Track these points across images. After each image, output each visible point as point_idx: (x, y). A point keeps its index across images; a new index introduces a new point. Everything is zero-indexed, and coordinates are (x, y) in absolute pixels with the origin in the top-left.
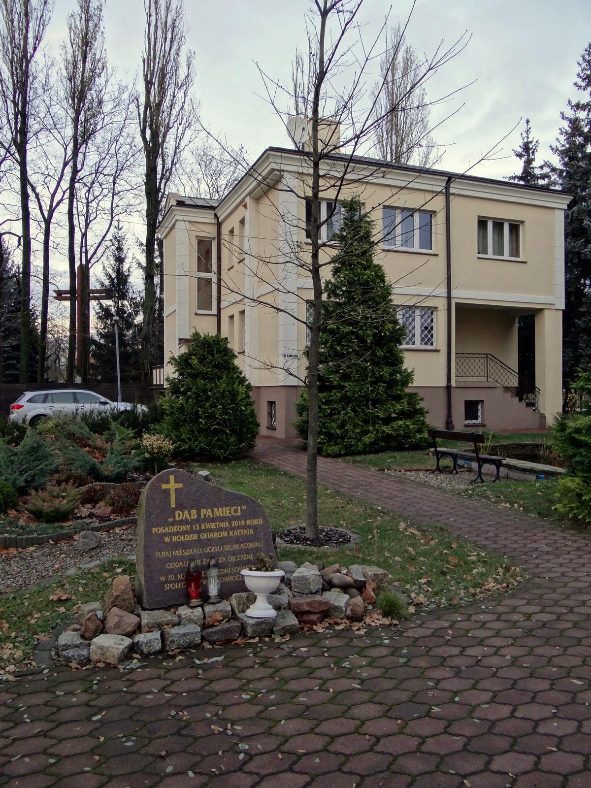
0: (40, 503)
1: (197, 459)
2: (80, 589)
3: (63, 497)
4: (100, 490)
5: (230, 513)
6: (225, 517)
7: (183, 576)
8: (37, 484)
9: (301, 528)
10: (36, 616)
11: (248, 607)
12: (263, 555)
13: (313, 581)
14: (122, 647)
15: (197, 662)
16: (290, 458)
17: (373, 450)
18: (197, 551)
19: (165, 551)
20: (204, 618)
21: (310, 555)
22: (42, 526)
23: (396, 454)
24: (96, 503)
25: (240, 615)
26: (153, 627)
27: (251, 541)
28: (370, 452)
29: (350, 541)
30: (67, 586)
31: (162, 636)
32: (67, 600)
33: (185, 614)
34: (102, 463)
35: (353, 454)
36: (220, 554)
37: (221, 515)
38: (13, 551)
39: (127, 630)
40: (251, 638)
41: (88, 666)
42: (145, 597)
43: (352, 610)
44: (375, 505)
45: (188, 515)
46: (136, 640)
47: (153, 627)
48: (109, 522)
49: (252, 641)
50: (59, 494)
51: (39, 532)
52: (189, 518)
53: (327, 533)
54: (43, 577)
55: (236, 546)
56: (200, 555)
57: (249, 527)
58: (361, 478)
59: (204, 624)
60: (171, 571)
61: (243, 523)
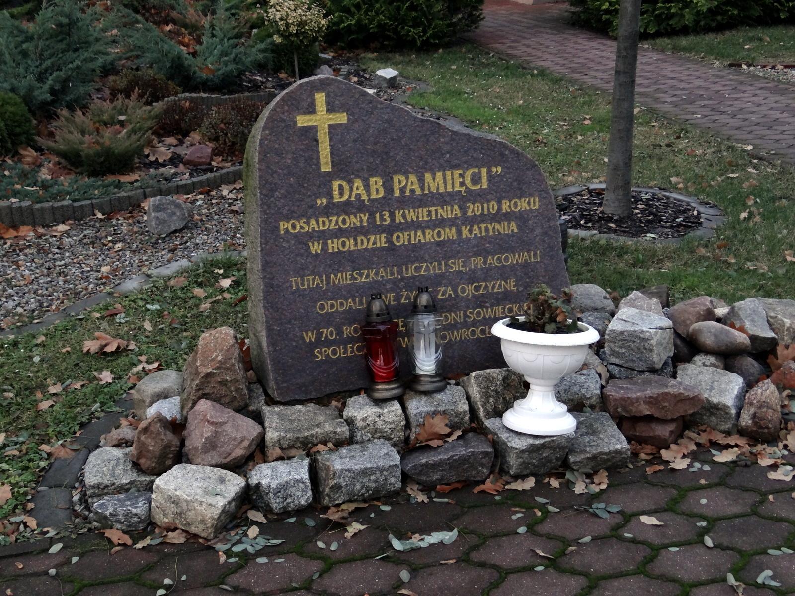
0: (76, 136)
1: (373, 45)
2: (147, 326)
3: (122, 124)
4: (191, 109)
5: (462, 184)
6: (450, 194)
7: (355, 330)
8: (72, 96)
9: (590, 192)
10: (52, 390)
11: (508, 405)
12: (549, 292)
13: (659, 343)
14: (220, 502)
15: (397, 545)
16: (548, 43)
17: (714, 25)
18: (384, 274)
19: (313, 273)
20: (408, 426)
21: (620, 256)
22: (80, 183)
23: (759, 32)
24: (186, 134)
25: (489, 423)
26: (291, 447)
27: (512, 250)
28: (707, 30)
29: (700, 224)
30: (120, 318)
31: (314, 472)
32: (118, 352)
33: (364, 419)
34: (194, 54)
35: (672, 33)
36: (438, 280)
37: (442, 190)
38: (27, 232)
39: (233, 456)
40: (516, 477)
41: (147, 541)
42: (271, 376)
43: (754, 416)
44: (738, 141)
45: (361, 190)
46: (254, 481)
47: (291, 447)
48: (209, 175)
49: (519, 486)
50: (112, 118)
51: (76, 195)
52: (364, 197)
53: (647, 202)
54: (77, 294)
55: (477, 262)
56: (394, 282)
57: (508, 217)
58: (697, 83)
59: (407, 439)
60: (328, 320)
61: (493, 207)
